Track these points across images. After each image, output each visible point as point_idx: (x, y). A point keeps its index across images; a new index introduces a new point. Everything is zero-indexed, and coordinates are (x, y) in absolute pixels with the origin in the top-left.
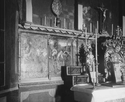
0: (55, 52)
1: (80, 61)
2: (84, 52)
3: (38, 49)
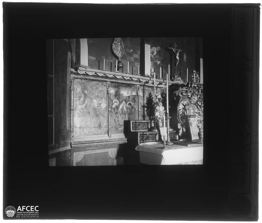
1: (147, 114)
2: (152, 103)
3: (95, 99)
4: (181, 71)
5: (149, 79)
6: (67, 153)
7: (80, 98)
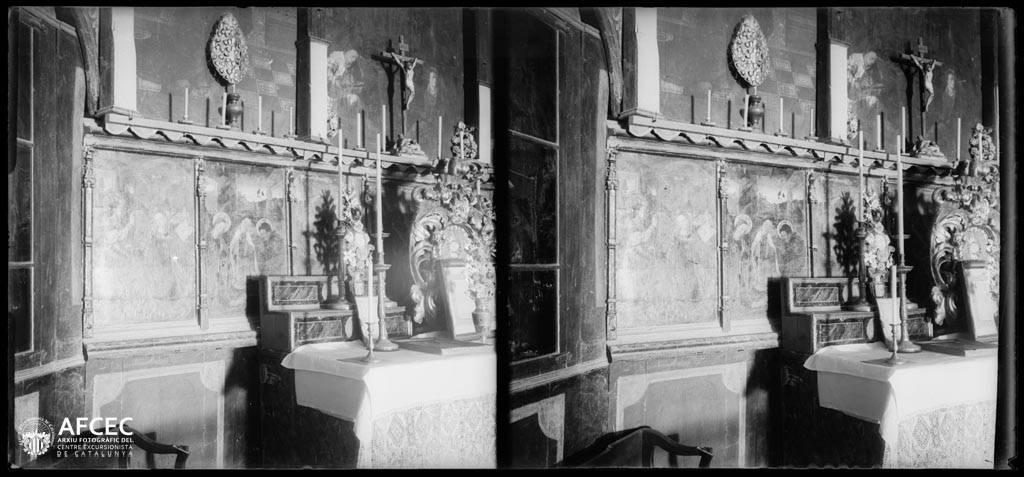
0: (222, 223)
1: (319, 255)
2: (333, 221)
3: (681, 213)
4: (420, 125)
5: (885, 158)
6: (72, 376)
7: (112, 207)
